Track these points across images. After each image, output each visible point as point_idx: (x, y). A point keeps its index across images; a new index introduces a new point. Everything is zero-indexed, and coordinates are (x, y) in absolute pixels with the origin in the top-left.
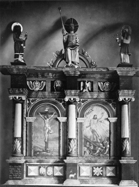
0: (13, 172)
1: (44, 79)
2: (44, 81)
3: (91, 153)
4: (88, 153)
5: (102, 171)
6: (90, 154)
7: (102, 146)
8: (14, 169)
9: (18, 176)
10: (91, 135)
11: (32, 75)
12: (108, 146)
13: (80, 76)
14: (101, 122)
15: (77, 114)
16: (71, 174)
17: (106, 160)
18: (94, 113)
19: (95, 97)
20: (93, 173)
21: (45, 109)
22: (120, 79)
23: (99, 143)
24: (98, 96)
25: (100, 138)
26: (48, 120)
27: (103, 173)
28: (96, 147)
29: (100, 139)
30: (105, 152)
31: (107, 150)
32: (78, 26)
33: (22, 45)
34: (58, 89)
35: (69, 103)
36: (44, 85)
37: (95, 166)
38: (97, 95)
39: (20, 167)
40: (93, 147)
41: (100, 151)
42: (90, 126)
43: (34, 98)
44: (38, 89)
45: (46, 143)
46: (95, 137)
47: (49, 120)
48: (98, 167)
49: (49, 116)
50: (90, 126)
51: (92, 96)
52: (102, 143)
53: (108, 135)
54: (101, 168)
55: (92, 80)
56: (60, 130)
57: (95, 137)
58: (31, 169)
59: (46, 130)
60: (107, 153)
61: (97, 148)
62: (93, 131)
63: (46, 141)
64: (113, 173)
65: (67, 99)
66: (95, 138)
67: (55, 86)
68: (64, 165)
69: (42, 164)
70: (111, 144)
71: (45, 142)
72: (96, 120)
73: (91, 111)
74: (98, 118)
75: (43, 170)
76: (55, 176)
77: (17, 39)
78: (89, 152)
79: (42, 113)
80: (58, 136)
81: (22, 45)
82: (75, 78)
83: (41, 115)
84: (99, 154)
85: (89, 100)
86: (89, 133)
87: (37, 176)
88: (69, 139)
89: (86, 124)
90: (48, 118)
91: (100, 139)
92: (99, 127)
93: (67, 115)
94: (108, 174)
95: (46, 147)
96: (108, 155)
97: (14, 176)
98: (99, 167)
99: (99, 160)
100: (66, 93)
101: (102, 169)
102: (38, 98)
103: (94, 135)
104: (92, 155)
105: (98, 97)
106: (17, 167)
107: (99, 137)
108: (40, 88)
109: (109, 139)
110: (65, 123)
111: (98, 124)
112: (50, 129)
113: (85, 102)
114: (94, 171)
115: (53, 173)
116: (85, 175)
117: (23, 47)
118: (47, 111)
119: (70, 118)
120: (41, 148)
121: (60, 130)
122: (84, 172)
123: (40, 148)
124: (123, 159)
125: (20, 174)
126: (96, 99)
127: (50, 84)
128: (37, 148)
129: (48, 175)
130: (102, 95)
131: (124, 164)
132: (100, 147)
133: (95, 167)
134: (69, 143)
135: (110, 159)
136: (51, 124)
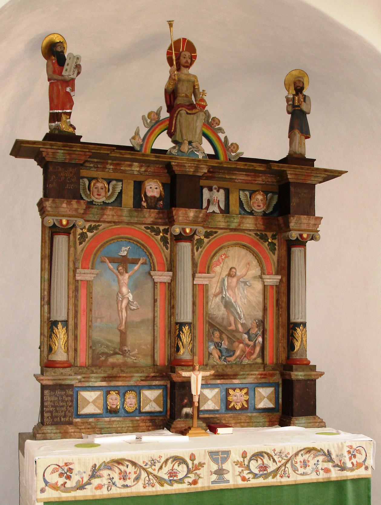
0: (52, 406)
1: (118, 175)
2: (118, 180)
3: (223, 357)
4: (217, 357)
5: (246, 397)
6: (220, 358)
7: (247, 341)
8: (56, 399)
9: (65, 416)
10: (223, 314)
11: (92, 165)
12: (260, 339)
13: (206, 177)
14: (245, 283)
15: (194, 265)
16: (186, 406)
17: (257, 373)
18: (230, 263)
19: (233, 226)
20: (228, 403)
21: (120, 250)
22: (292, 189)
23: (240, 332)
24: (240, 224)
25: (243, 321)
26: (127, 276)
27: (250, 403)
28: (234, 342)
29: (242, 325)
30: (252, 354)
31: (258, 349)
32: (195, 57)
33: (68, 89)
34: (153, 203)
35: (180, 238)
36: (118, 190)
37: (232, 386)
38: (238, 221)
39: (71, 393)
40: (227, 343)
41: (243, 351)
42: (221, 292)
43: (94, 221)
44: (104, 199)
45: (123, 334)
46: (232, 319)
47: (129, 277)
48: (239, 388)
49: (129, 265)
50: (221, 292)
51: (227, 222)
52: (248, 333)
53: (259, 314)
54: (245, 391)
55: (226, 184)
56: (155, 301)
57: (232, 319)
58: (88, 398)
59: (122, 301)
60: (258, 357)
61: (236, 343)
62: (228, 305)
63: (123, 328)
64: (270, 400)
65: (177, 230)
66: (233, 322)
67: (146, 196)
68: (163, 385)
69: (113, 384)
70: (265, 336)
71: (120, 330)
72: (235, 280)
73: (223, 257)
74: (238, 274)
75: (114, 400)
76: (259, 409)
77: (56, 77)
78: (220, 354)
79: (113, 260)
80: (150, 316)
81: (68, 89)
82: (194, 179)
83: (110, 265)
84: (240, 359)
85: (220, 231)
86: (219, 310)
87: (100, 414)
88: (177, 323)
89: (214, 289)
90: (127, 272)
91: (242, 325)
92: (240, 295)
93: (172, 267)
94: (260, 403)
95: (123, 342)
96: (259, 360)
97: (57, 417)
98: (241, 389)
99: (242, 373)
100: (176, 214)
101: (247, 394)
102: (104, 222)
103: (230, 315)
104: (225, 360)
105: (239, 225)
106: (63, 393)
107: (240, 319)
108: (109, 197)
109: (262, 323)
110: (167, 284)
111: (239, 289)
112: (131, 298)
113: (211, 237)
114: (230, 398)
115: (140, 406)
116: (211, 408)
117: (70, 95)
118: (125, 253)
119: (180, 274)
120: (110, 344)
121: (155, 301)
122: (210, 402)
123: (107, 347)
124: (296, 370)
125: (69, 412)
126: (235, 230)
127: (132, 188)
128: (101, 346)
129: (127, 412)
130: (249, 223)
131: (299, 381)
132: (243, 343)
133: (232, 389)
134: (179, 334)
135: (264, 370)
136: (135, 287)
